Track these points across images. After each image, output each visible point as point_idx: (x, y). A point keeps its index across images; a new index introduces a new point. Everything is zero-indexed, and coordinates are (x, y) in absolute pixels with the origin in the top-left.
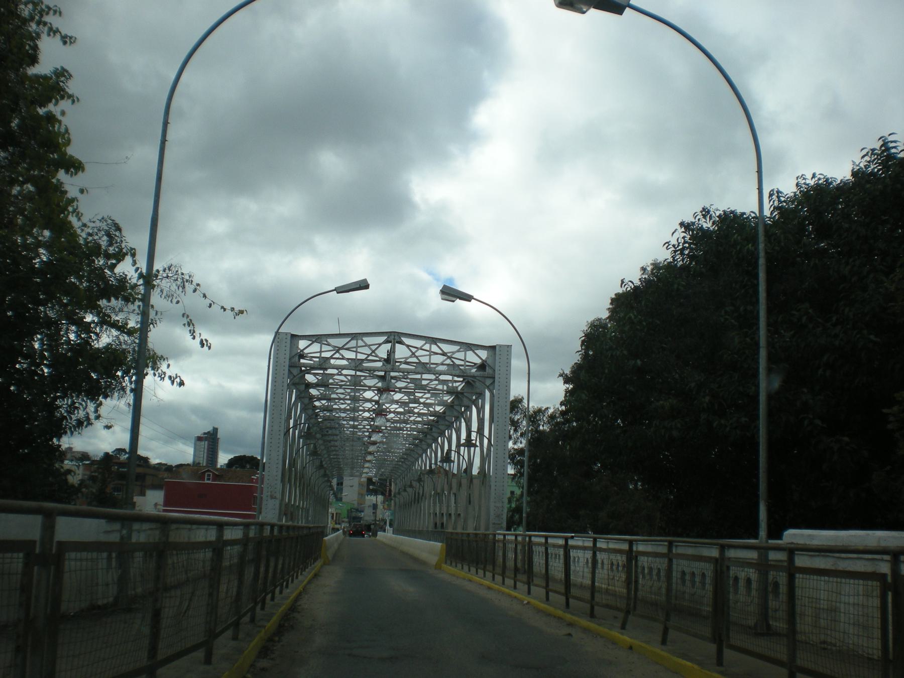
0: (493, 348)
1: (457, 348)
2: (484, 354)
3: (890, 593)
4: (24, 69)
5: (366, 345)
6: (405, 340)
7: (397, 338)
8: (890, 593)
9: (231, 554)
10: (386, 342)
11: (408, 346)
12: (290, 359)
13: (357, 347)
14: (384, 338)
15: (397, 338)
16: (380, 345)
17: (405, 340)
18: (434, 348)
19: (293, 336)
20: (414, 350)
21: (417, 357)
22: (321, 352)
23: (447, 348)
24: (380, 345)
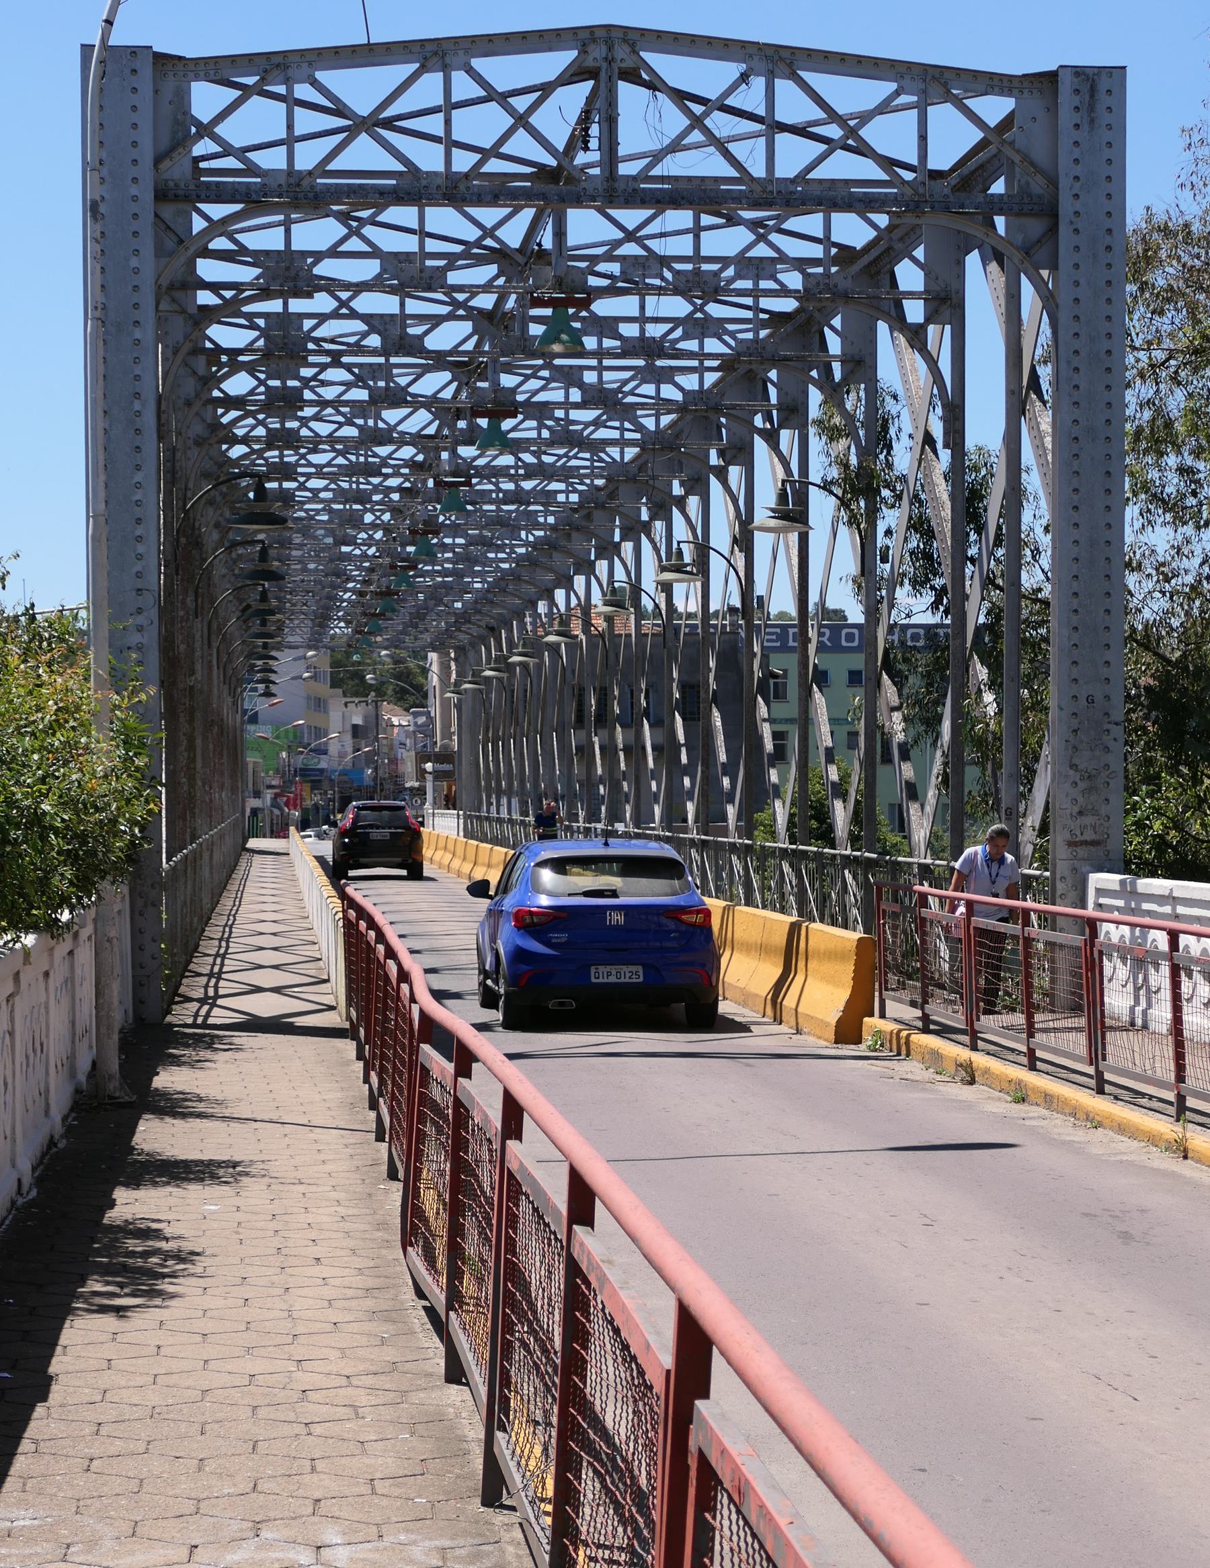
0: (1049, 79)
1: (731, 70)
2: (994, 108)
3: (394, 182)
4: (902, 986)
5: (492, 95)
6: (655, 60)
7: (621, 52)
8: (394, 182)
9: (204, 847)
10: (571, 76)
11: (681, 97)
12: (158, 160)
13: (449, 107)
14: (562, 59)
15: (621, 52)
16: (546, 90)
17: (655, 60)
18: (792, 105)
19: (163, 60)
20: (698, 109)
21: (492, 95)
22: (290, 141)
23: (851, 94)
24: (546, 90)
